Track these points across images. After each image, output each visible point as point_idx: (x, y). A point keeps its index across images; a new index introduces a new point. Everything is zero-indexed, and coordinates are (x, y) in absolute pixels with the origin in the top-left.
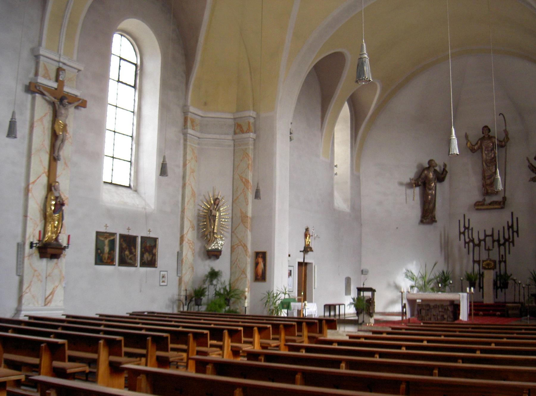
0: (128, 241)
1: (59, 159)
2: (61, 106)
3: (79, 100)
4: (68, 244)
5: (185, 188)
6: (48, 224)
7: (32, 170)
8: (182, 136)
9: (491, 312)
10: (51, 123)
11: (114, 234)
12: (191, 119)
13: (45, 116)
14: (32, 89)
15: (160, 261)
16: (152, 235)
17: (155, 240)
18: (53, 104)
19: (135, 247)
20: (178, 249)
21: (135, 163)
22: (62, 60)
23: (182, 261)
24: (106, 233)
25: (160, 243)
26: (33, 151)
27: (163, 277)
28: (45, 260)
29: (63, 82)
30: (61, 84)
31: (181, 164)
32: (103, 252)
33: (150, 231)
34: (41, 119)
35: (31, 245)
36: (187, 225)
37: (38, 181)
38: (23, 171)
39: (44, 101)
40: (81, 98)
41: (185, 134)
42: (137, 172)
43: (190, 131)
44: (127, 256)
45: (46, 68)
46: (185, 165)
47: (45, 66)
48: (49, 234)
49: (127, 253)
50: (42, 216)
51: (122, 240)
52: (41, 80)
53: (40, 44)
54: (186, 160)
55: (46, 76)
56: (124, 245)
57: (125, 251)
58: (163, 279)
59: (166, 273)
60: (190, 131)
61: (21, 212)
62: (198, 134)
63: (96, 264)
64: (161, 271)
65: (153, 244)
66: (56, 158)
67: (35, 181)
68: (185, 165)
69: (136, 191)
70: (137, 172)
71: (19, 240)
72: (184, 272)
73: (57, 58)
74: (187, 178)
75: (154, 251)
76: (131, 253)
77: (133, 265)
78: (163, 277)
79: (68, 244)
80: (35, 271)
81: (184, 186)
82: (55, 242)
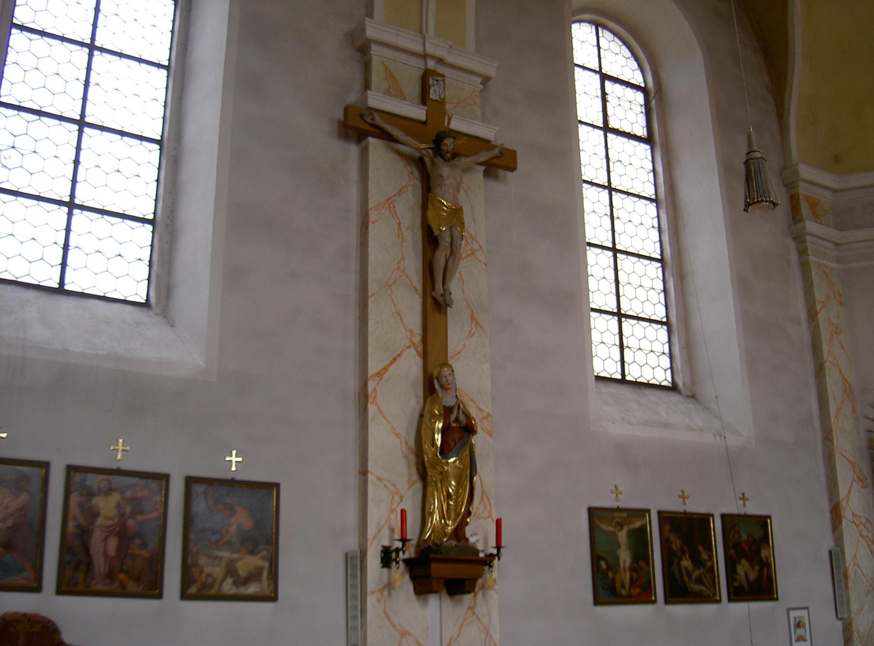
0: (687, 529)
1: (448, 305)
2: (439, 160)
3: (494, 147)
4: (498, 547)
5: (824, 376)
6: (430, 489)
7: (371, 339)
8: (792, 245)
9: (451, 503)
10: (419, 213)
11: (642, 513)
12: (807, 198)
13: (399, 193)
14: (359, 127)
15: (783, 583)
16: (753, 509)
17: (762, 522)
18: (419, 163)
19: (708, 547)
20: (828, 543)
21: (678, 323)
22: (430, 50)
23: (845, 575)
24: (618, 510)
25: (778, 530)
26: (372, 288)
27: (799, 625)
28: (433, 601)
29: (441, 103)
30: (436, 108)
31: (803, 315)
32: (614, 566)
33: (744, 498)
34: (389, 203)
35: (387, 557)
36: (845, 474)
37: (392, 368)
38: (352, 346)
39: (393, 156)
40: (498, 143)
41: (799, 239)
42: (689, 348)
43: (811, 226)
44: (689, 575)
45: (390, 75)
46: (812, 316)
47: (387, 69)
48: (436, 516)
49: (686, 563)
50: (414, 470)
51: (667, 527)
52: (377, 100)
53: (370, 14)
54: (814, 302)
55: (395, 91)
56: (676, 543)
57: (680, 559)
58: (800, 632)
59: (804, 613)
60: (811, 226)
61: (353, 463)
62: (834, 234)
63: (597, 602)
64: (789, 610)
65: (758, 534)
66: (440, 299)
67: (386, 369)
68: (812, 316)
69: (693, 397)
70: (689, 348)
71: (352, 543)
72: (854, 607)
73: (417, 47)
74: (825, 346)
75: (764, 553)
76: (698, 562)
77: (710, 598)
78: (799, 625)
79: (498, 547)
80: (404, 634)
81: (819, 370)
82: (454, 543)
